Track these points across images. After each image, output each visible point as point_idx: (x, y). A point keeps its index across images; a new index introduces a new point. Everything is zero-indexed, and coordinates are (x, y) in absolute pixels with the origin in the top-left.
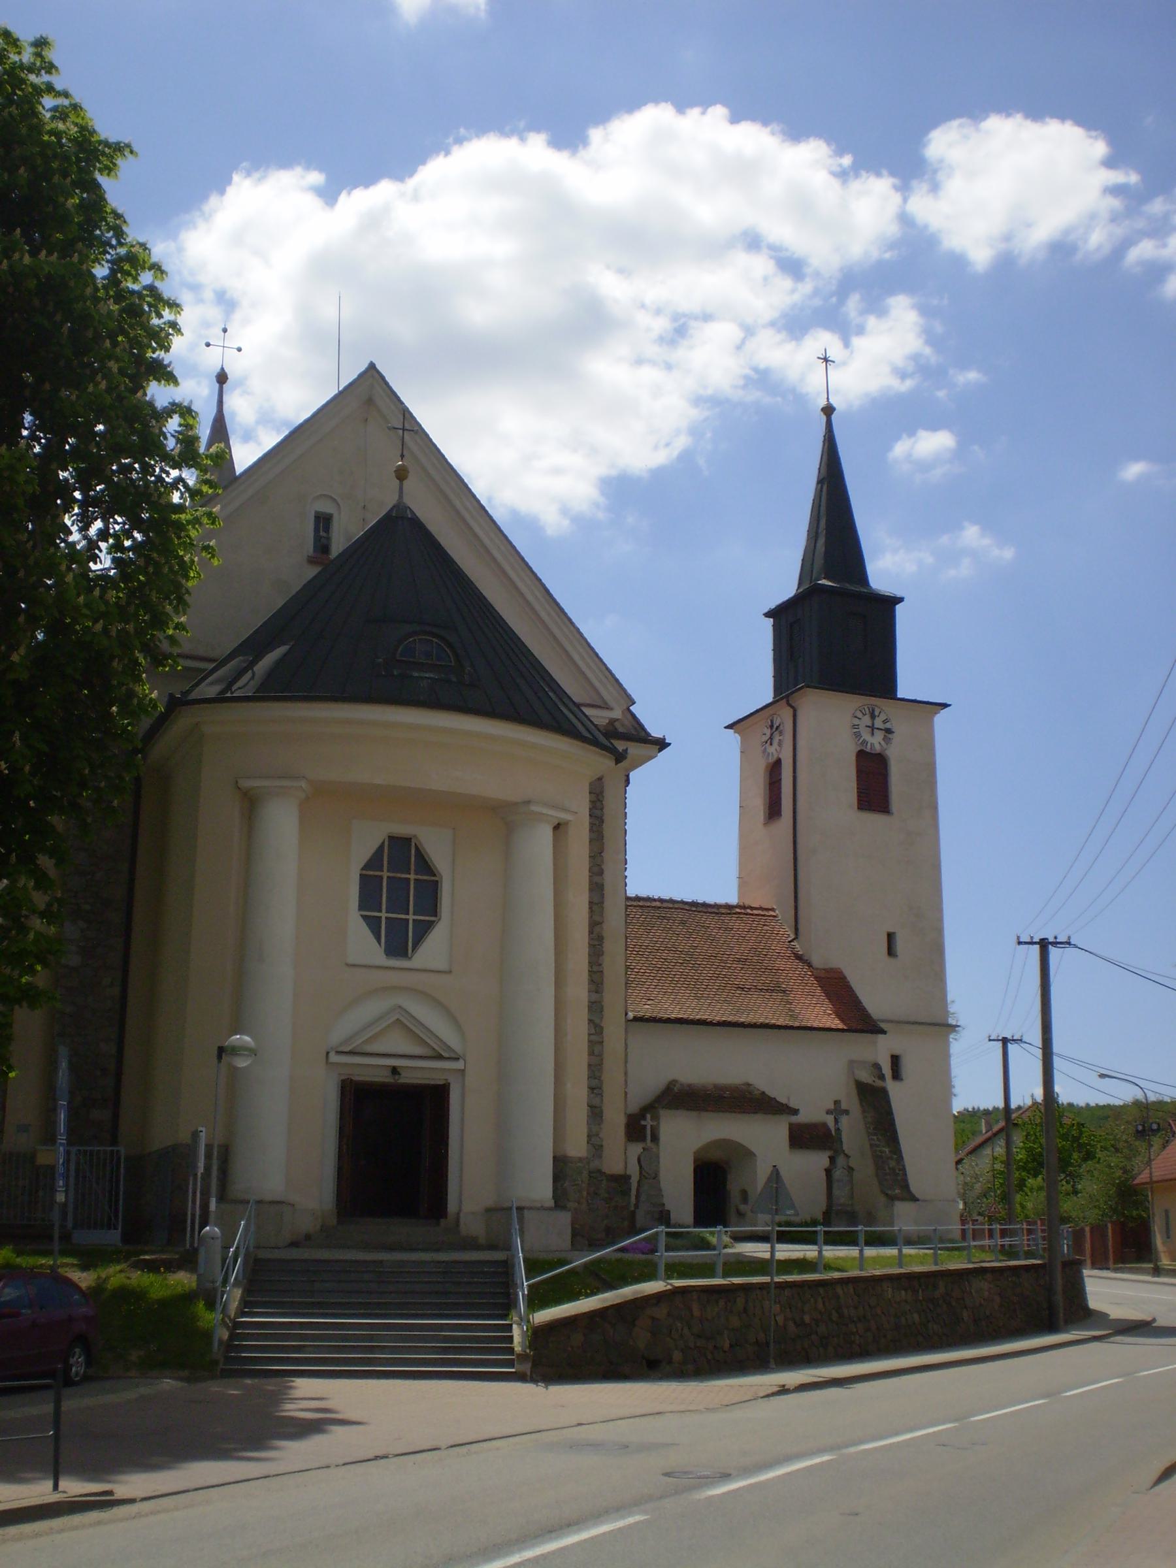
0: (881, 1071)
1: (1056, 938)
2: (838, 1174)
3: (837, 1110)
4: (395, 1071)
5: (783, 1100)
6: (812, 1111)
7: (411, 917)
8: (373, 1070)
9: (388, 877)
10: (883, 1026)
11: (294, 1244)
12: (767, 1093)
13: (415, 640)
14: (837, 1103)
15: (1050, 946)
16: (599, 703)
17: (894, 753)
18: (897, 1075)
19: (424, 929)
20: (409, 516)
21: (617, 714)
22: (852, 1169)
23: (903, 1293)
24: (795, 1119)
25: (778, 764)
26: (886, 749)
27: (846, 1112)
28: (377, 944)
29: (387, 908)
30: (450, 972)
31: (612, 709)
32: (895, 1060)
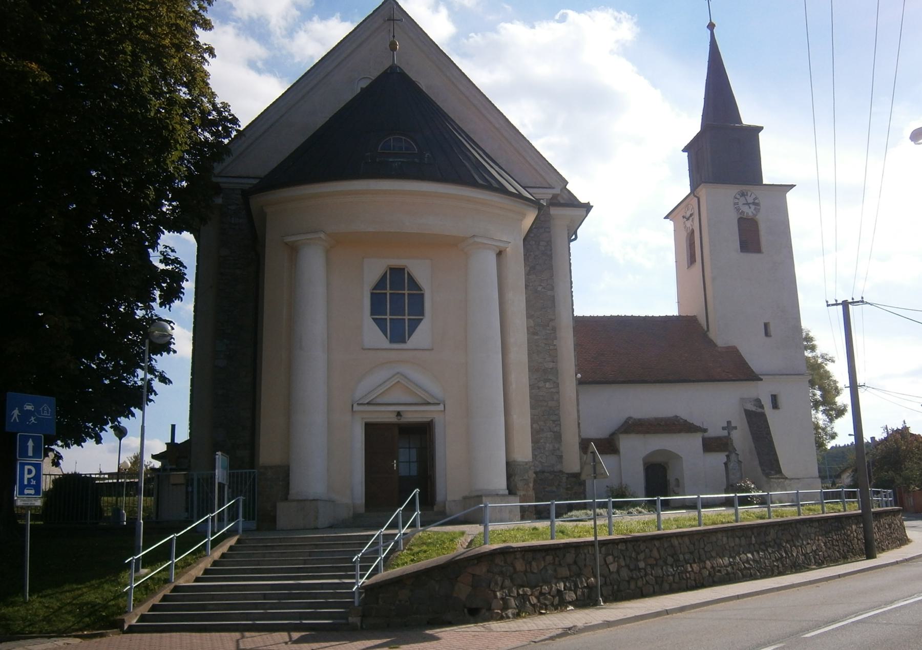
0: (761, 403)
1: (853, 299)
2: (731, 465)
3: (729, 427)
4: (399, 414)
5: (698, 424)
6: (715, 430)
7: (406, 317)
8: (385, 415)
9: (390, 294)
10: (762, 377)
11: (332, 527)
12: (688, 420)
13: (390, 139)
14: (729, 423)
15: (850, 305)
16: (547, 186)
17: (761, 218)
18: (775, 405)
19: (414, 324)
20: (398, 71)
21: (557, 191)
22: (741, 462)
23: (737, 539)
24: (706, 435)
25: (693, 231)
26: (756, 215)
27: (735, 428)
28: (385, 338)
29: (390, 312)
30: (432, 349)
31: (554, 188)
32: (774, 399)
